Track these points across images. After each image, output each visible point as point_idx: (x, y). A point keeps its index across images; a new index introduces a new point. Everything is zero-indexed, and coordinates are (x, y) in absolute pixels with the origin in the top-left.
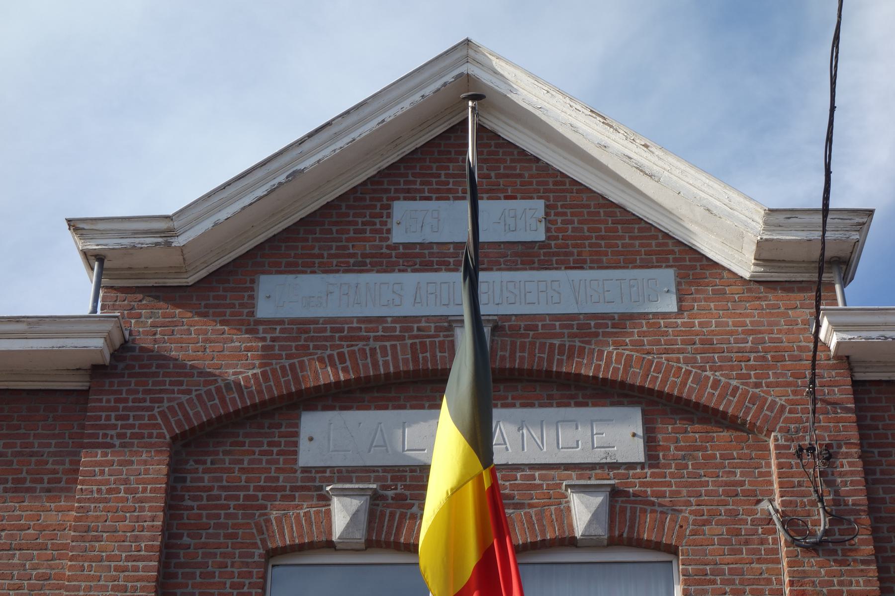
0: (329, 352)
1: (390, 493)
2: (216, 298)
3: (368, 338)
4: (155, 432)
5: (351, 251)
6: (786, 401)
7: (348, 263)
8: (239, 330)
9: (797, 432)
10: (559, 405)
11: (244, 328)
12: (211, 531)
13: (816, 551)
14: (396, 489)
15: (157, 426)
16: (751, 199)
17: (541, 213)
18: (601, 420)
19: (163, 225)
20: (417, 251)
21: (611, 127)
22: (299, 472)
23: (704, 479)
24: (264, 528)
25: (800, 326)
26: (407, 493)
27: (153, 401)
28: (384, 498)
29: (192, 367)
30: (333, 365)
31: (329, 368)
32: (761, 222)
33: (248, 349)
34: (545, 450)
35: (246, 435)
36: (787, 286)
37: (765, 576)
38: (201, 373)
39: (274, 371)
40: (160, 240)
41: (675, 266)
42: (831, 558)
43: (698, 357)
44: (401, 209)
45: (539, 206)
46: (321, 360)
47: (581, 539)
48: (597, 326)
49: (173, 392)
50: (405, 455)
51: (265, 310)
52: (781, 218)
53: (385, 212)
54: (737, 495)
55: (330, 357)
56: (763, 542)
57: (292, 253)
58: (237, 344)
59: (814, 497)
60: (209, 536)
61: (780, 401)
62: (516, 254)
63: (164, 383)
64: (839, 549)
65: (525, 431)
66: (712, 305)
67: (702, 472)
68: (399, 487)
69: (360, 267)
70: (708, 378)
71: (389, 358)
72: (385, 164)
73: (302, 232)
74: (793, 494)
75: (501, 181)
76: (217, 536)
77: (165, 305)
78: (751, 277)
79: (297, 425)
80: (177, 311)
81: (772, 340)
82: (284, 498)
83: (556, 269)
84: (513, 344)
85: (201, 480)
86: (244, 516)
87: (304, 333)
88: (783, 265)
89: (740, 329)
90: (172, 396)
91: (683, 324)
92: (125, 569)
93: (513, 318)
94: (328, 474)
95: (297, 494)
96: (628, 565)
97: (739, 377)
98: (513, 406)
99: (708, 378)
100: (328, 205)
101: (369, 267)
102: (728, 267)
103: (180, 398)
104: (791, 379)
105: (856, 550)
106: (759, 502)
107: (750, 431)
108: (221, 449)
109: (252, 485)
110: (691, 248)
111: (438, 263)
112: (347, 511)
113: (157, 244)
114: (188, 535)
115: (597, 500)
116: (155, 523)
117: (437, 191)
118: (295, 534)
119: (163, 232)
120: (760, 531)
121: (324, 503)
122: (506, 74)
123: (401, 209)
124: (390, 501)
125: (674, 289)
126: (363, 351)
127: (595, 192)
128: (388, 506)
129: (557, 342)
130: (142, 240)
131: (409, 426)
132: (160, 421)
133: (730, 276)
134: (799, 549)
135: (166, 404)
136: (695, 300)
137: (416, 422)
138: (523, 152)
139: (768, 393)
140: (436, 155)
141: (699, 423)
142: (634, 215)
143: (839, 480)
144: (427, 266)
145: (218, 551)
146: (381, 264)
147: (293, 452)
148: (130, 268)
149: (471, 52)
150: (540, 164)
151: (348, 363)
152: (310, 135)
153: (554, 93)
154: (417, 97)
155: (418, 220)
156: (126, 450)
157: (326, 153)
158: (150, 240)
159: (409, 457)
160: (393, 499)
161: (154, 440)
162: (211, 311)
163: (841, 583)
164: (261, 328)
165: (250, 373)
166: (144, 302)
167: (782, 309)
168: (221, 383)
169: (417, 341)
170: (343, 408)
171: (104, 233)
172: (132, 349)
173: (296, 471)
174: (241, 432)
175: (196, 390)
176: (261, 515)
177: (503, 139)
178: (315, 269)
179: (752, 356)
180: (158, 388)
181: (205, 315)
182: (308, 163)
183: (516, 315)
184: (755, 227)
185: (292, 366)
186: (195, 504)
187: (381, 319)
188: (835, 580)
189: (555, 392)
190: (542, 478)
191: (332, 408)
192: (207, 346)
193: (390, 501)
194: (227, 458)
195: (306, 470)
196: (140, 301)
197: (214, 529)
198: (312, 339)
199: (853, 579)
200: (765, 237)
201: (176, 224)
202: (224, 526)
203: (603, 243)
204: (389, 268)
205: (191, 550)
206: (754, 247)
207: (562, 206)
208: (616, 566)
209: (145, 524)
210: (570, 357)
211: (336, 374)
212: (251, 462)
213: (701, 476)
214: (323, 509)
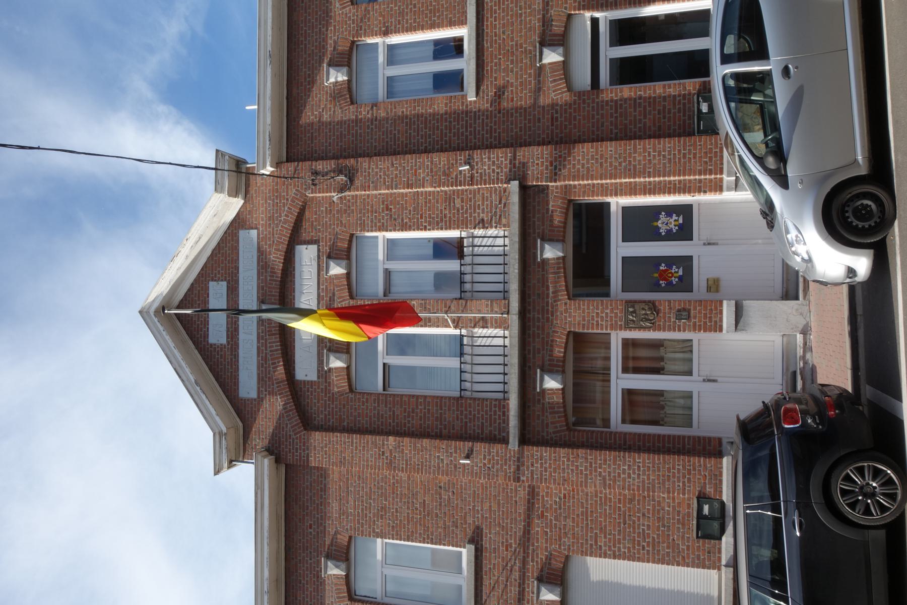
36: (247, 186)
44: (212, 340)
46: (274, 372)
51: (253, 395)
52: (219, 187)
56: (349, 201)
61: (294, 191)
72: (193, 346)
87: (264, 379)
100: (210, 369)
107: (306, 203)
123: (212, 340)
138: (189, 290)
152: (180, 377)
154: (164, 333)
157: (188, 370)
184: (223, 197)
187: (258, 348)
195: (318, 377)
201: (217, 431)
204: (237, 345)
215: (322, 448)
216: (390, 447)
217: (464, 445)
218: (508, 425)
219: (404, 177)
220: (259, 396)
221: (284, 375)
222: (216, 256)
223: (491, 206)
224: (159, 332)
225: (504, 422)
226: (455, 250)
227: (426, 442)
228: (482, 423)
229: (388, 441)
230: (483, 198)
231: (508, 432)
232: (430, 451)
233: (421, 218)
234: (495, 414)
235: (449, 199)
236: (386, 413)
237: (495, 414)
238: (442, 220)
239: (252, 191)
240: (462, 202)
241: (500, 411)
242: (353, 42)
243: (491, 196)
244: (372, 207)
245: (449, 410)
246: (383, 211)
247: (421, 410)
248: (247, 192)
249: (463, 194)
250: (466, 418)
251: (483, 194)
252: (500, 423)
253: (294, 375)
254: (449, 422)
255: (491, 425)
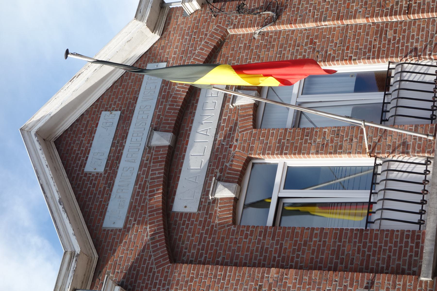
0: (147, 197)
1: (218, 174)
2: (108, 246)
3: (146, 181)
4: (166, 270)
5: (102, 189)
6: (215, 25)
7: (107, 190)
8: (126, 235)
9: (229, 22)
10: (195, 109)
11: (126, 233)
12: (218, 249)
13: (279, 15)
14: (217, 172)
15: (163, 270)
16: (128, 24)
17: (108, 113)
18: (206, 93)
19: (68, 256)
20: (110, 162)
21: (80, 74)
22: (199, 212)
23: (240, 57)
24: (222, 226)
25: (185, 20)
26: (220, 167)
27: (150, 272)
28: (220, 177)
29: (138, 255)
30: (154, 195)
31: (155, 197)
32: (139, 22)
33: (137, 231)
34: (214, 114)
35: (177, 235)
36: (167, 24)
37: (285, 36)
38: (143, 251)
39: (150, 220)
40: (75, 259)
41: (147, 63)
42: (283, 10)
43: (188, 55)
44: (89, 168)
45: (103, 113)
46: (150, 200)
47: (236, 195)
48: (165, 92)
49: (148, 263)
50: (203, 168)
51: (120, 224)
52: (139, 15)
53: (88, 175)
54: (250, 46)
55: (150, 196)
56: (271, 37)
57: (96, 213)
58: (133, 236)
59: (257, 16)
60: (220, 249)
61: (215, 27)
62: (124, 123)
63: (143, 267)
64: (280, 8)
65: (203, 122)
66: (167, 50)
67: (237, 58)
68: (217, 171)
69: (111, 186)
70: (198, 52)
71: (157, 172)
72: (65, 175)
73: (87, 210)
74: (254, 23)
75: (88, 129)
76: (221, 246)
77: (105, 268)
78: (159, 35)
79: (178, 213)
80: (109, 263)
81: (188, 29)
82: (210, 218)
83: (135, 107)
84: (164, 123)
85: (193, 253)
86: (215, 234)
87: (136, 210)
88: (157, 24)
89: (181, 40)
90: (150, 263)
91: (173, 60)
92: (229, 281)
93: (152, 123)
94: (203, 200)
95: (210, 212)
96: (266, 108)
97: (201, 41)
98: (191, 127)
99: (198, 52)
100: (78, 199)
101: (112, 182)
102: (153, 44)
103: (152, 260)
104: (207, 23)
105: (282, 3)
106: (254, 38)
107: (224, 40)
108: (181, 245)
109: (201, 231)
110: (140, 57)
111: (119, 153)
112: (222, 190)
113: (76, 260)
114: (218, 258)
115: (220, 186)
116: (210, 268)
117: (85, 154)
118: (228, 212)
119: (71, 257)
120: (267, 38)
121: (216, 201)
122: (42, 116)
123: (89, 168)
124: (222, 174)
125: (157, 64)
126: (151, 183)
127: (105, 93)
128: (224, 175)
129: (168, 107)
130: (72, 267)
131: (190, 167)
132: (161, 268)
133: (157, 44)
134: (277, 21)
135: (154, 266)
136: (164, 56)
137: (189, 165)
138: (77, 120)
139: (210, 31)
140: (67, 155)
141: (216, 59)
142: (119, 78)
143: (252, 8)
144: (119, 159)
145: (228, 245)
146: (112, 176)
147: (189, 215)
148: (82, 283)
149: (26, 129)
150: (85, 114)
151: (155, 189)
152: (44, 193)
153: (57, 96)
154: (40, 152)
155: (95, 163)
156: (171, 283)
157: (54, 189)
158: (73, 264)
159: (204, 167)
160: (221, 173)
161: (170, 270)
162: (114, 248)
163: (294, 7)
164: (128, 226)
165: (148, 230)
166: (101, 278)
167: (176, 26)
168: (150, 242)
169: (152, 161)
170: (175, 194)
171: (63, 284)
172: (123, 282)
173: (199, 214)
174: (175, 237)
175: (151, 253)
176: (216, 227)
177: (69, 128)
178: (106, 204)
179: (193, 36)
180: (145, 270)
181: (115, 250)
182: (57, 196)
183: (151, 122)
184: (142, 26)
185: (149, 212)
186: (204, 256)
187: (138, 176)
188: (292, 9)
189: (189, 111)
190: (225, 116)
191: (173, 199)
192: (130, 249)
193: (222, 174)
194: (186, 243)
195: (199, 209)
196: (100, 280)
197: (218, 247)
198: (139, 204)
199: (293, 3)
200: (146, 21)
201: (69, 250)
202: (217, 242)
203: (128, 90)
204: (115, 173)
205: (225, 257)
206: (148, 29)
207: (107, 105)
208: (264, 115)
209: (209, 272)
210: (176, 102)
211: (159, 194)
212: (190, 232)
213: (239, 58)
214: (219, 201)
215: (187, 282)
216: (271, 281)
217: (363, 277)
218: (421, 258)
219: (335, 10)
220: (125, 227)
221: (161, 199)
222: (116, 87)
223: (427, 36)
224: (35, 150)
225: (416, 255)
226: (382, 82)
227: (316, 274)
228: (389, 257)
229: (268, 273)
230: (419, 29)
231: (420, 267)
232: (319, 284)
233: (348, 49)
234: (406, 246)
235: (381, 30)
236: (272, 246)
237: (406, 246)
238: (370, 51)
239: (170, 29)
240: (395, 33)
241: (412, 242)
242: (249, 159)
243: (428, 27)
244: (295, 41)
245: (350, 242)
246: (306, 45)
247: (315, 242)
248: (162, 35)
249: (396, 26)
250: (369, 250)
251: (419, 25)
252: (411, 256)
253: (171, 207)
254: (348, 255)
255: (399, 259)
